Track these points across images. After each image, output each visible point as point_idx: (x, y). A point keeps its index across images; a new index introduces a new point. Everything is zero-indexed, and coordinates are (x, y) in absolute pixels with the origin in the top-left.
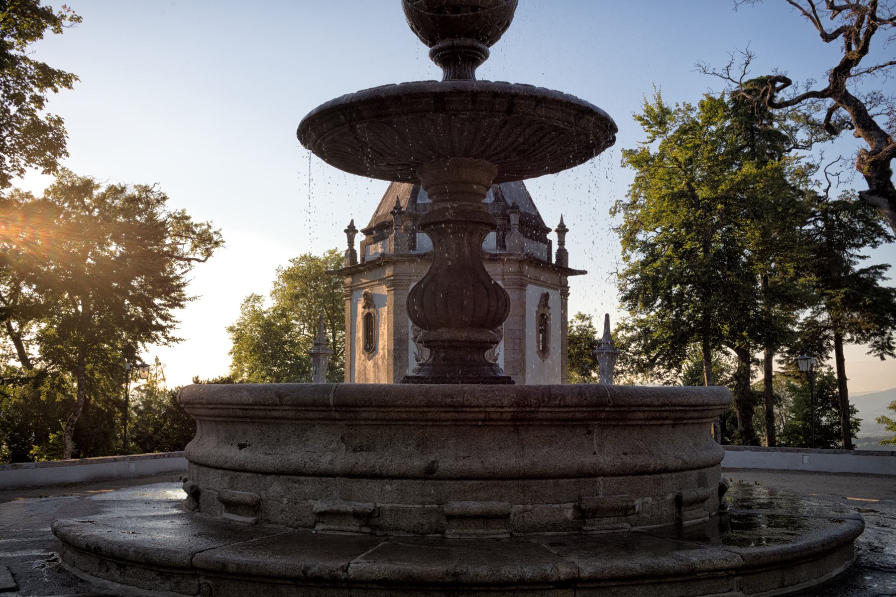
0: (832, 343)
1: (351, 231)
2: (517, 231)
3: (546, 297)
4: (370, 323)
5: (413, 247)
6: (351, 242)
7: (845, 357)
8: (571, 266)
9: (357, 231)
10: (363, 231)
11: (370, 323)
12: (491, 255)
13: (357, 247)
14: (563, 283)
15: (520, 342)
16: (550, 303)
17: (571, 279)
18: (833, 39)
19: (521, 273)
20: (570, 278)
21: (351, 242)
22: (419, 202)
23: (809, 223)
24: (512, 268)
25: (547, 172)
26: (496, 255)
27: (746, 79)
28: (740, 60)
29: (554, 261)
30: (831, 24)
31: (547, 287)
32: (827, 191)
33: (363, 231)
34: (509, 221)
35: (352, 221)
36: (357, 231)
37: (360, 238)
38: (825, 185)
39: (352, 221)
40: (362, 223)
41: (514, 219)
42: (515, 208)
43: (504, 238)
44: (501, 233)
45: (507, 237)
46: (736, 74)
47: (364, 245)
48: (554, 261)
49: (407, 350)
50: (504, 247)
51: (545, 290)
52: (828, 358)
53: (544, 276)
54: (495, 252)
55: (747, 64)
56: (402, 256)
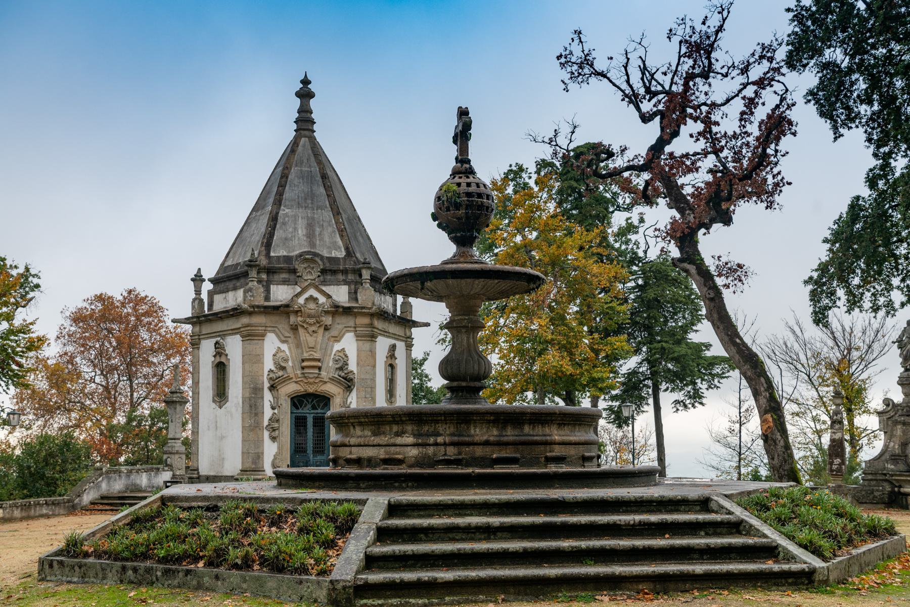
0: (650, 391)
1: (198, 279)
2: (368, 285)
3: (393, 348)
4: (221, 369)
5: (267, 298)
6: (198, 292)
7: (661, 405)
8: (415, 318)
9: (204, 280)
10: (209, 280)
11: (221, 369)
12: (343, 307)
13: (204, 296)
14: (408, 334)
15: (372, 391)
16: (397, 354)
17: (415, 331)
18: (650, 121)
19: (371, 325)
20: (413, 330)
21: (198, 292)
22: (272, 254)
23: (630, 280)
24: (366, 320)
25: (725, 310)
26: (349, 308)
27: (571, 147)
28: (565, 130)
29: (399, 313)
30: (647, 106)
31: (395, 339)
32: (645, 252)
33: (209, 280)
34: (360, 276)
35: (199, 269)
36: (204, 280)
37: (207, 286)
38: (643, 247)
39: (199, 269)
40: (209, 272)
41: (366, 274)
42: (366, 264)
43: (356, 292)
44: (353, 287)
45: (359, 291)
46: (562, 141)
47: (211, 294)
48: (399, 313)
49: (263, 398)
50: (356, 300)
51: (393, 342)
52: (648, 404)
53: (393, 329)
54: (347, 305)
55: (573, 132)
56: (258, 307)
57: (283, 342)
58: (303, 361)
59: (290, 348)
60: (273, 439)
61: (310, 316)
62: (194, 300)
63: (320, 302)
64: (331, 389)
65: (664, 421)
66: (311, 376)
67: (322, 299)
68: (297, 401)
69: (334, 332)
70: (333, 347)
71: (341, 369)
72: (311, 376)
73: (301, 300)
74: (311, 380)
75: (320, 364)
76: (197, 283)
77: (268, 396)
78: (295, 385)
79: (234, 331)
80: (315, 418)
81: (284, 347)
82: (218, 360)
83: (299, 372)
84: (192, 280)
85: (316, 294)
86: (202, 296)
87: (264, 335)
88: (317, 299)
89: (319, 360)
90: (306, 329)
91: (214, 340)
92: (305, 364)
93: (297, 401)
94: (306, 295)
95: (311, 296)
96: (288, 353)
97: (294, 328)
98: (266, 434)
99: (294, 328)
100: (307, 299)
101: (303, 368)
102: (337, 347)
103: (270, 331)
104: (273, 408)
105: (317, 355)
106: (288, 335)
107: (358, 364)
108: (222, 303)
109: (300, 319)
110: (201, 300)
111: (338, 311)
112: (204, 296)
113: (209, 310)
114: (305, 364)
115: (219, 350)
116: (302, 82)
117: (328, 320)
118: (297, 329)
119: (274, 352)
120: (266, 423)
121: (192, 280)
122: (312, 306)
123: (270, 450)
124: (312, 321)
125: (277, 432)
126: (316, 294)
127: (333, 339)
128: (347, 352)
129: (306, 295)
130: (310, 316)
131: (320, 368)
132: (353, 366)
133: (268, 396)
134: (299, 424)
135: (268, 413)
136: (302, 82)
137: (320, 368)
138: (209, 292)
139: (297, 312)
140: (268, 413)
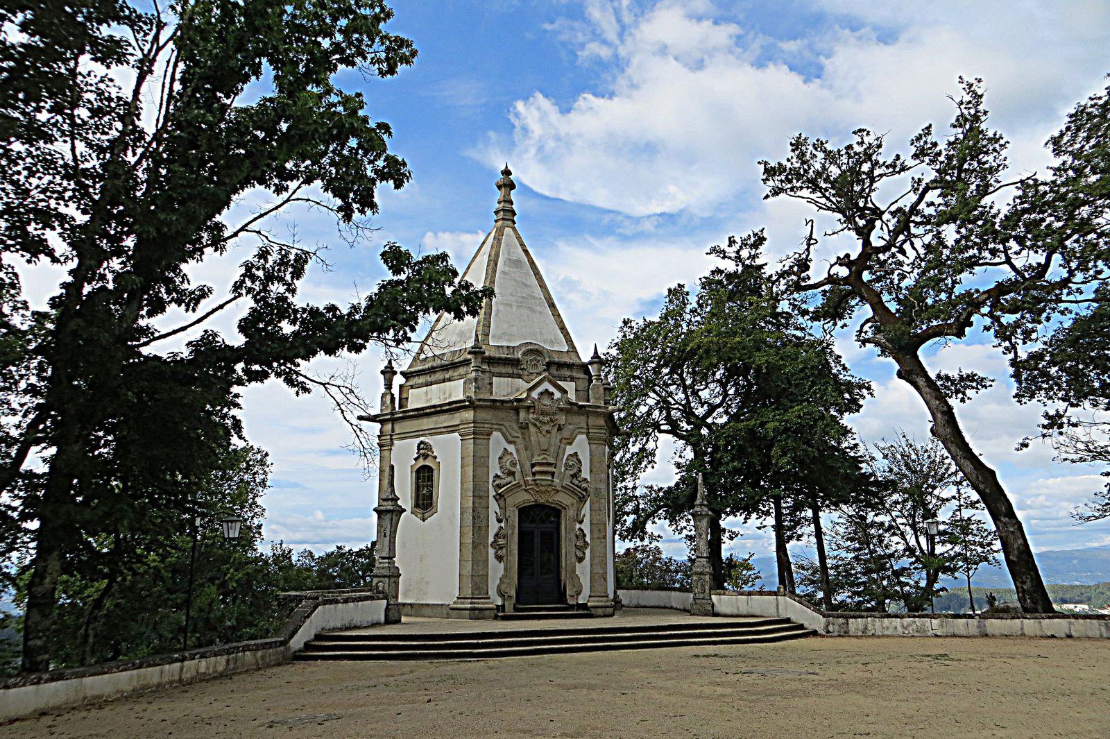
6: (389, 386)
9: (395, 373)
10: (402, 373)
21: (389, 386)
33: (402, 373)
36: (395, 373)
57: (510, 442)
58: (533, 465)
59: (517, 450)
60: (499, 558)
61: (543, 413)
62: (384, 395)
63: (555, 397)
64: (563, 499)
65: (652, 604)
66: (544, 483)
67: (557, 395)
68: (524, 512)
69: (566, 433)
70: (565, 450)
71: (574, 476)
72: (544, 483)
73: (535, 394)
74: (543, 489)
75: (554, 470)
76: (388, 376)
77: (494, 506)
78: (525, 493)
79: (451, 429)
80: (543, 534)
81: (511, 448)
82: (421, 462)
83: (530, 478)
84: (382, 372)
85: (552, 389)
86: (393, 391)
87: (489, 434)
88: (553, 394)
89: (549, 464)
90: (538, 428)
92: (536, 469)
93: (524, 512)
94: (540, 389)
95: (547, 390)
96: (515, 455)
97: (524, 427)
98: (491, 552)
99: (524, 427)
100: (541, 394)
101: (534, 474)
102: (570, 450)
103: (496, 430)
104: (499, 521)
105: (551, 460)
106: (516, 434)
107: (591, 471)
108: (417, 399)
109: (531, 416)
110: (392, 395)
111: (573, 409)
112: (395, 391)
113: (400, 407)
114: (536, 469)
115: (424, 451)
116: (503, 173)
117: (562, 419)
118: (527, 428)
119: (500, 453)
120: (491, 539)
121: (382, 372)
122: (546, 401)
123: (496, 570)
124: (547, 419)
125: (504, 550)
126: (552, 389)
127: (564, 441)
128: (580, 457)
129: (540, 389)
130: (543, 413)
131: (553, 474)
132: (585, 474)
133: (494, 506)
134: (525, 539)
135: (494, 527)
136: (503, 173)
137: (553, 474)
138: (401, 386)
139: (528, 408)
140: (494, 527)
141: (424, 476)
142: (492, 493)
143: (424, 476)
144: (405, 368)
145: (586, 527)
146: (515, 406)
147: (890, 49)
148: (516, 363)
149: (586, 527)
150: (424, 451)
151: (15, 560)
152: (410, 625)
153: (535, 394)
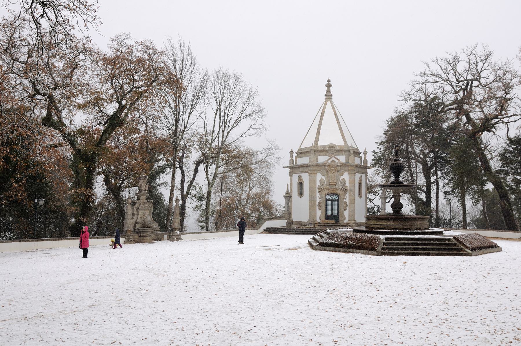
6: (292, 157)
10: (296, 153)
21: (292, 157)
33: (296, 153)
37: (295, 155)
60: (320, 209)
67: (337, 161)
69: (341, 172)
77: (318, 195)
81: (323, 178)
85: (335, 159)
91: (298, 175)
94: (331, 160)
98: (317, 208)
99: (327, 171)
102: (342, 177)
111: (342, 165)
112: (294, 158)
115: (300, 178)
120: (317, 204)
126: (335, 159)
129: (331, 160)
132: (347, 184)
135: (318, 200)
141: (301, 184)
142: (317, 191)
143: (301, 184)
144: (296, 151)
145: (347, 200)
146: (324, 165)
147: (224, 70)
148: (326, 151)
149: (347, 200)
150: (300, 178)
151: (509, 180)
152: (294, 227)
153: (329, 161)
